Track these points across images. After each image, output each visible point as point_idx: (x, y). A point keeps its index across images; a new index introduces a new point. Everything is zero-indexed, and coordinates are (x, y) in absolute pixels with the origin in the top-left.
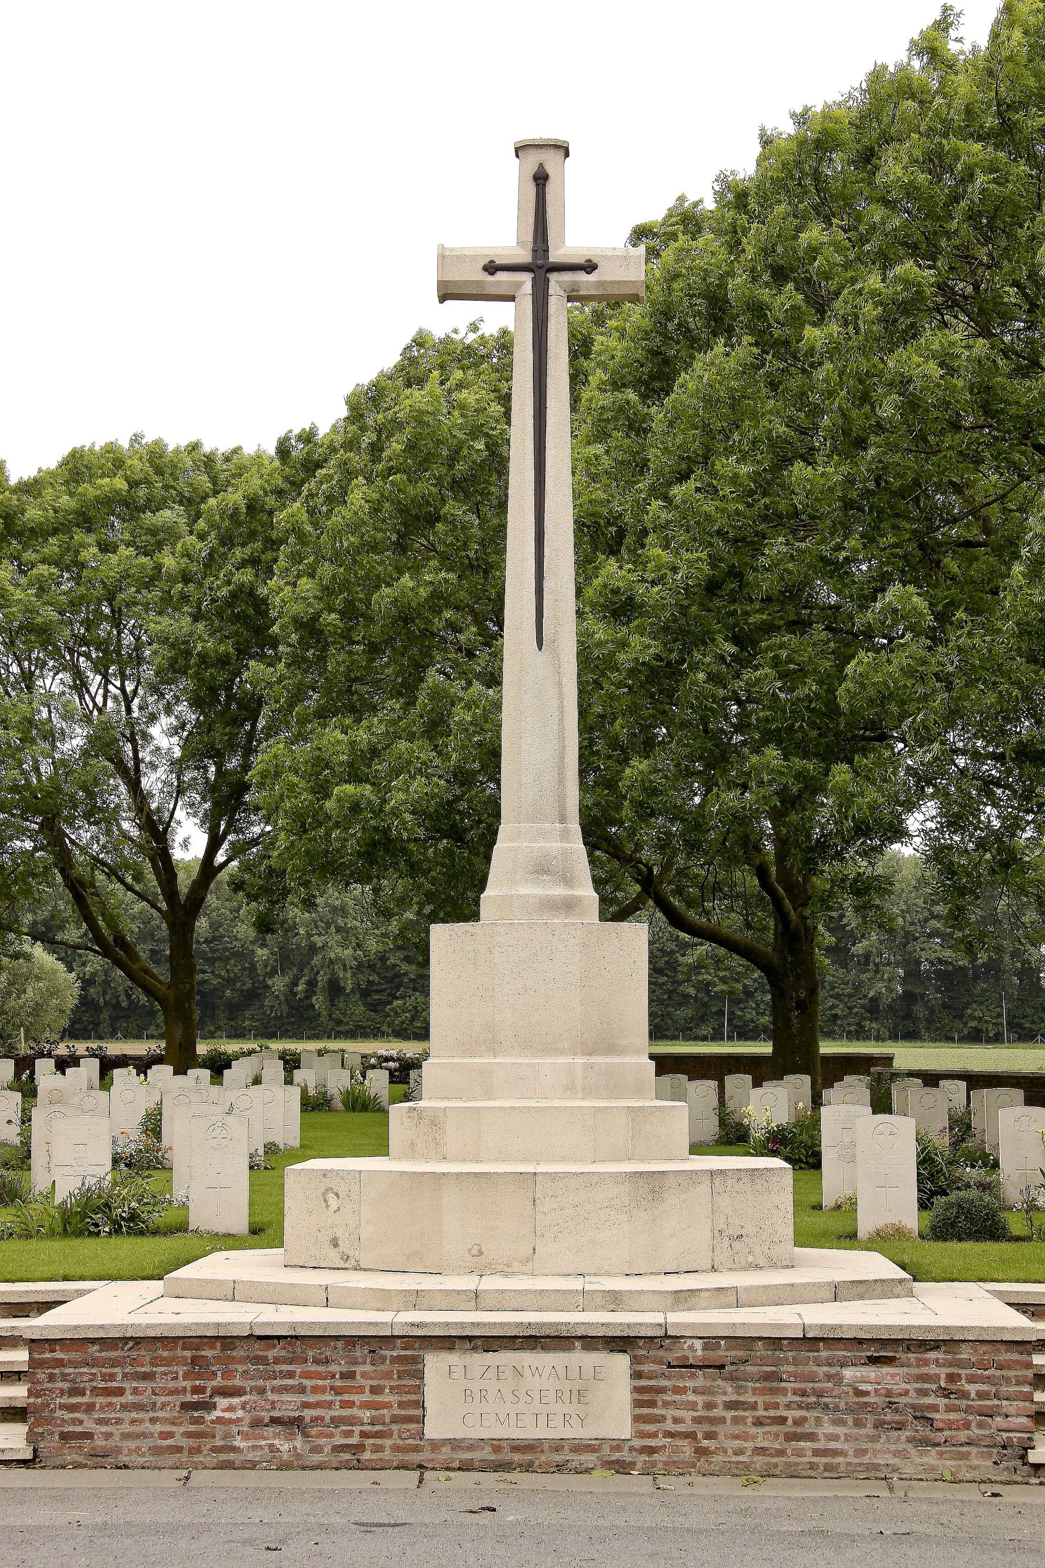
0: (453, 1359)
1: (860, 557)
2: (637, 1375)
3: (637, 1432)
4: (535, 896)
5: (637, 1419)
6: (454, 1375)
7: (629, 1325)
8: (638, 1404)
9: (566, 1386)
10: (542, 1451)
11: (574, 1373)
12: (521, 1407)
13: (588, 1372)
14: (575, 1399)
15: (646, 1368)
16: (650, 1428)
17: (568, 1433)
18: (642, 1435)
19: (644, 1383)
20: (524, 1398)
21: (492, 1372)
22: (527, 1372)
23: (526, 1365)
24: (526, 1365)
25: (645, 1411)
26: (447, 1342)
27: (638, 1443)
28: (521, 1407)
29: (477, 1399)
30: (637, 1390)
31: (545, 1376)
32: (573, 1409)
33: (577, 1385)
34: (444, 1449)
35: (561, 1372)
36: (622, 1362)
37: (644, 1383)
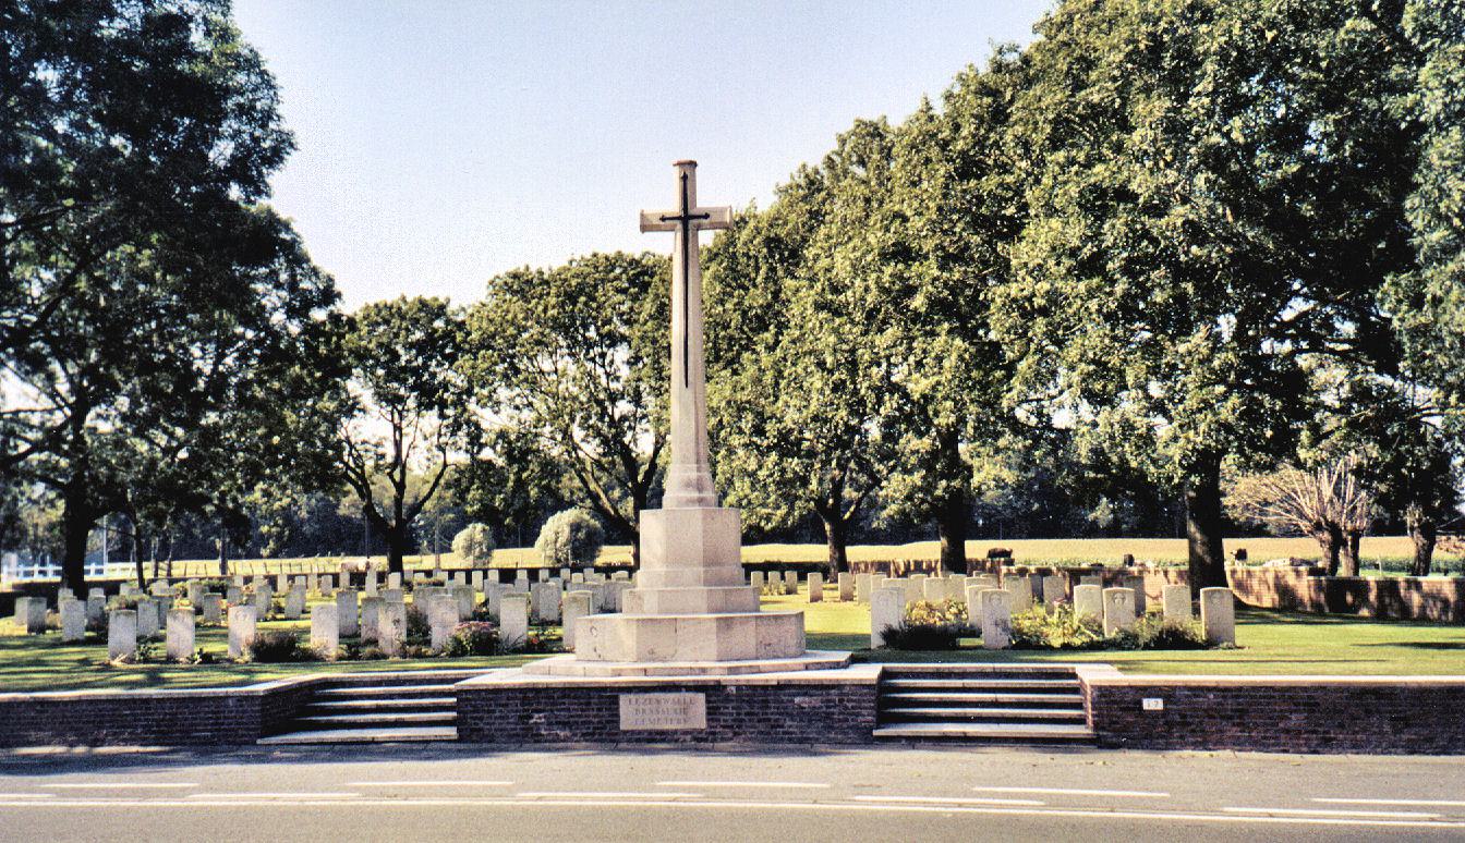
0: (632, 696)
2: (708, 702)
5: (708, 720)
8: (708, 714)
13: (688, 700)
17: (679, 727)
30: (708, 708)
32: (682, 717)
36: (701, 697)
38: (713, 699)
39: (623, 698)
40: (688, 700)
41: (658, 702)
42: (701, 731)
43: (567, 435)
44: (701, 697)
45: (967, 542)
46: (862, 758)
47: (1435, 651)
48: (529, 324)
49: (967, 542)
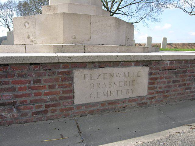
0: (86, 72)
2: (150, 74)
6: (87, 79)
8: (150, 83)
10: (119, 104)
15: (153, 71)
21: (102, 76)
22: (115, 75)
23: (115, 73)
26: (141, 103)
29: (96, 87)
30: (150, 79)
34: (83, 108)
35: (127, 75)
36: (147, 69)
44: (144, 71)
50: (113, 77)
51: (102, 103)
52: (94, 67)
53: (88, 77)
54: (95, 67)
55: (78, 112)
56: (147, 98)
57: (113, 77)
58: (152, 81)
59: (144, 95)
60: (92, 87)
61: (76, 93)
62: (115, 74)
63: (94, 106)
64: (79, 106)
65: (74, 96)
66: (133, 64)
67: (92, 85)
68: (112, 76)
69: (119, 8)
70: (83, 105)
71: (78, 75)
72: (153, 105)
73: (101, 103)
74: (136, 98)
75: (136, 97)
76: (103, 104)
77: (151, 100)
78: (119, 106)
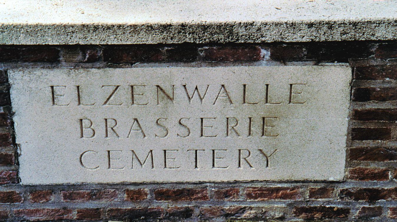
0: (60, 77)
1: (25, 195)
2: (359, 94)
3: (353, 172)
4: (4, 193)
5: (353, 155)
6: (60, 100)
7: (355, 24)
8: (355, 134)
9: (242, 113)
10: (204, 198)
11: (256, 93)
12: (171, 140)
13: (279, 91)
14: (256, 128)
15: (377, 85)
16: (374, 166)
17: (244, 174)
18: (362, 175)
19: (371, 106)
20: (174, 129)
21: (123, 95)
22: (180, 93)
23: (178, 84)
24: (178, 84)
25: (370, 144)
26: (45, 55)
27: (352, 186)
28: (171, 140)
29: (100, 131)
30: (357, 115)
31: (208, 99)
32: (256, 142)
33: (262, 110)
34: (53, 198)
35: (236, 94)
36: (338, 77)
37: (371, 106)
38: (377, 85)
39: (26, 85)
40: (279, 91)
41: (164, 94)
42: (325, 188)
43: (128, 214)
44: (338, 77)
45: (30, 173)
46: (16, 129)
47: (203, 123)
48: (26, 28)
49: (30, 173)
50: (172, 99)
51: (132, 188)
52: (89, 61)
53: (67, 95)
54: (93, 60)
55: (37, 211)
56: (347, 193)
57: (172, 99)
58: (365, 128)
59: (331, 179)
60: (87, 132)
61: (23, 147)
62: (180, 93)
63: (100, 198)
64: (40, 192)
65: (17, 155)
66: (265, 53)
67: (86, 123)
68: (168, 97)
69: (196, 91)
70: (52, 189)
71: (26, 85)
72: (164, 128)
73: (128, 190)
74: (285, 185)
75: (287, 182)
76: (134, 192)
77: (370, 203)
78: (206, 206)
